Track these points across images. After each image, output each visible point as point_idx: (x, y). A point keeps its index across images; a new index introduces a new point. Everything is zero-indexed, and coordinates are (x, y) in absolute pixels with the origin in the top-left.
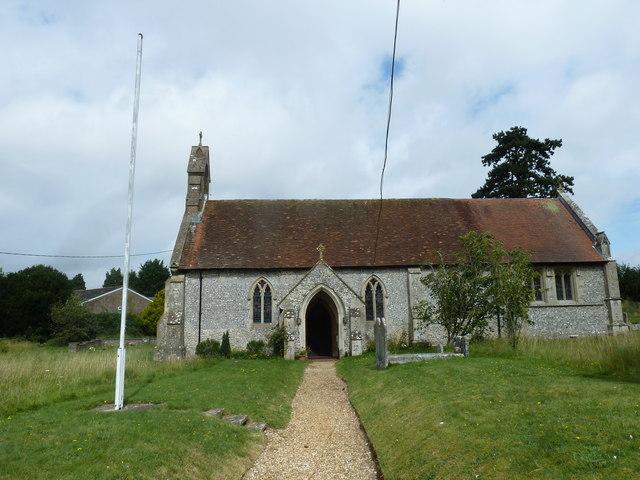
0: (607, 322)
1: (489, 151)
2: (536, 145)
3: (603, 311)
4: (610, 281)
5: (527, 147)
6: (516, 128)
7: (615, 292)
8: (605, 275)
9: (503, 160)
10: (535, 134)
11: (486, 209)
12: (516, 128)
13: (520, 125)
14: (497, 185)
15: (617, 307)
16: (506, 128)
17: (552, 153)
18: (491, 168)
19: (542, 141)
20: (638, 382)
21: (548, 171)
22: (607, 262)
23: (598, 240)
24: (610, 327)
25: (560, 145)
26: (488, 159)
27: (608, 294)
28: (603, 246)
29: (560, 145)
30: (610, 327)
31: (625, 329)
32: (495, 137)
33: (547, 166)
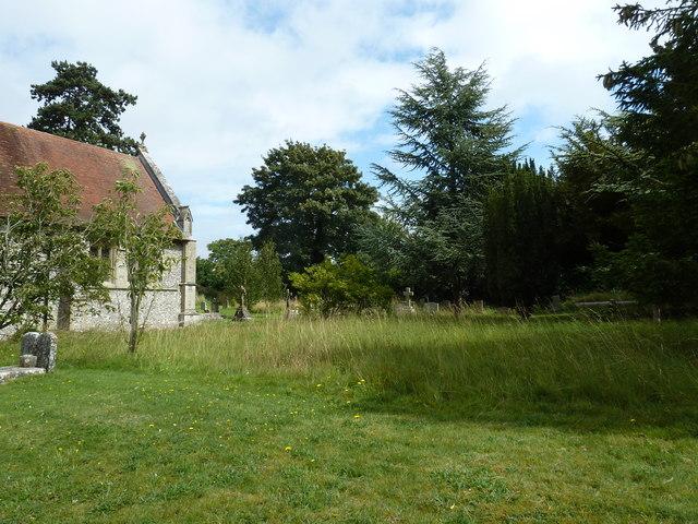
0: (179, 311)
1: (41, 82)
2: (107, 95)
3: (176, 297)
4: (188, 269)
5: (94, 91)
6: (85, 64)
7: (191, 277)
8: (184, 254)
9: (59, 100)
10: (108, 79)
11: (44, 148)
12: (85, 64)
13: (91, 62)
14: (48, 120)
15: (191, 293)
16: (73, 61)
17: (123, 110)
18: (42, 104)
19: (115, 90)
20: (695, 436)
21: (115, 130)
22: (187, 241)
23: (182, 214)
24: (181, 317)
25: (134, 103)
26: (39, 91)
27: (183, 277)
28: (186, 223)
29: (134, 103)
30: (181, 317)
31: (196, 318)
32: (54, 65)
33: (115, 122)
